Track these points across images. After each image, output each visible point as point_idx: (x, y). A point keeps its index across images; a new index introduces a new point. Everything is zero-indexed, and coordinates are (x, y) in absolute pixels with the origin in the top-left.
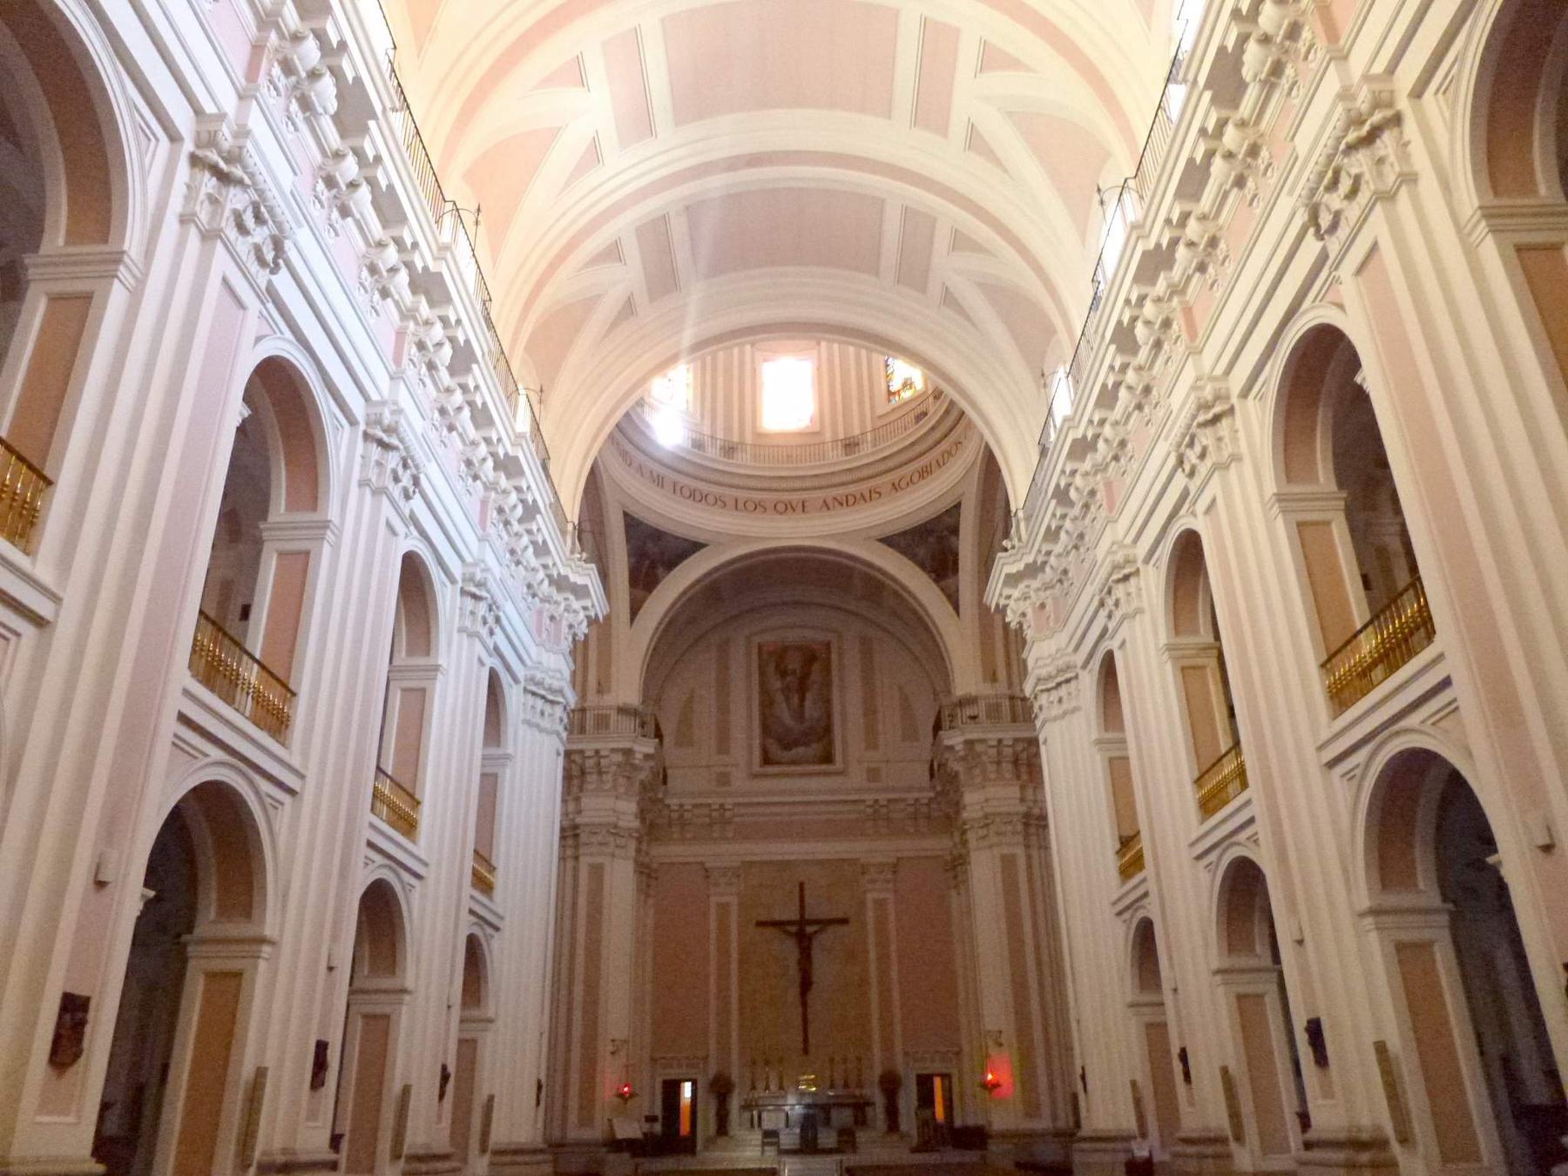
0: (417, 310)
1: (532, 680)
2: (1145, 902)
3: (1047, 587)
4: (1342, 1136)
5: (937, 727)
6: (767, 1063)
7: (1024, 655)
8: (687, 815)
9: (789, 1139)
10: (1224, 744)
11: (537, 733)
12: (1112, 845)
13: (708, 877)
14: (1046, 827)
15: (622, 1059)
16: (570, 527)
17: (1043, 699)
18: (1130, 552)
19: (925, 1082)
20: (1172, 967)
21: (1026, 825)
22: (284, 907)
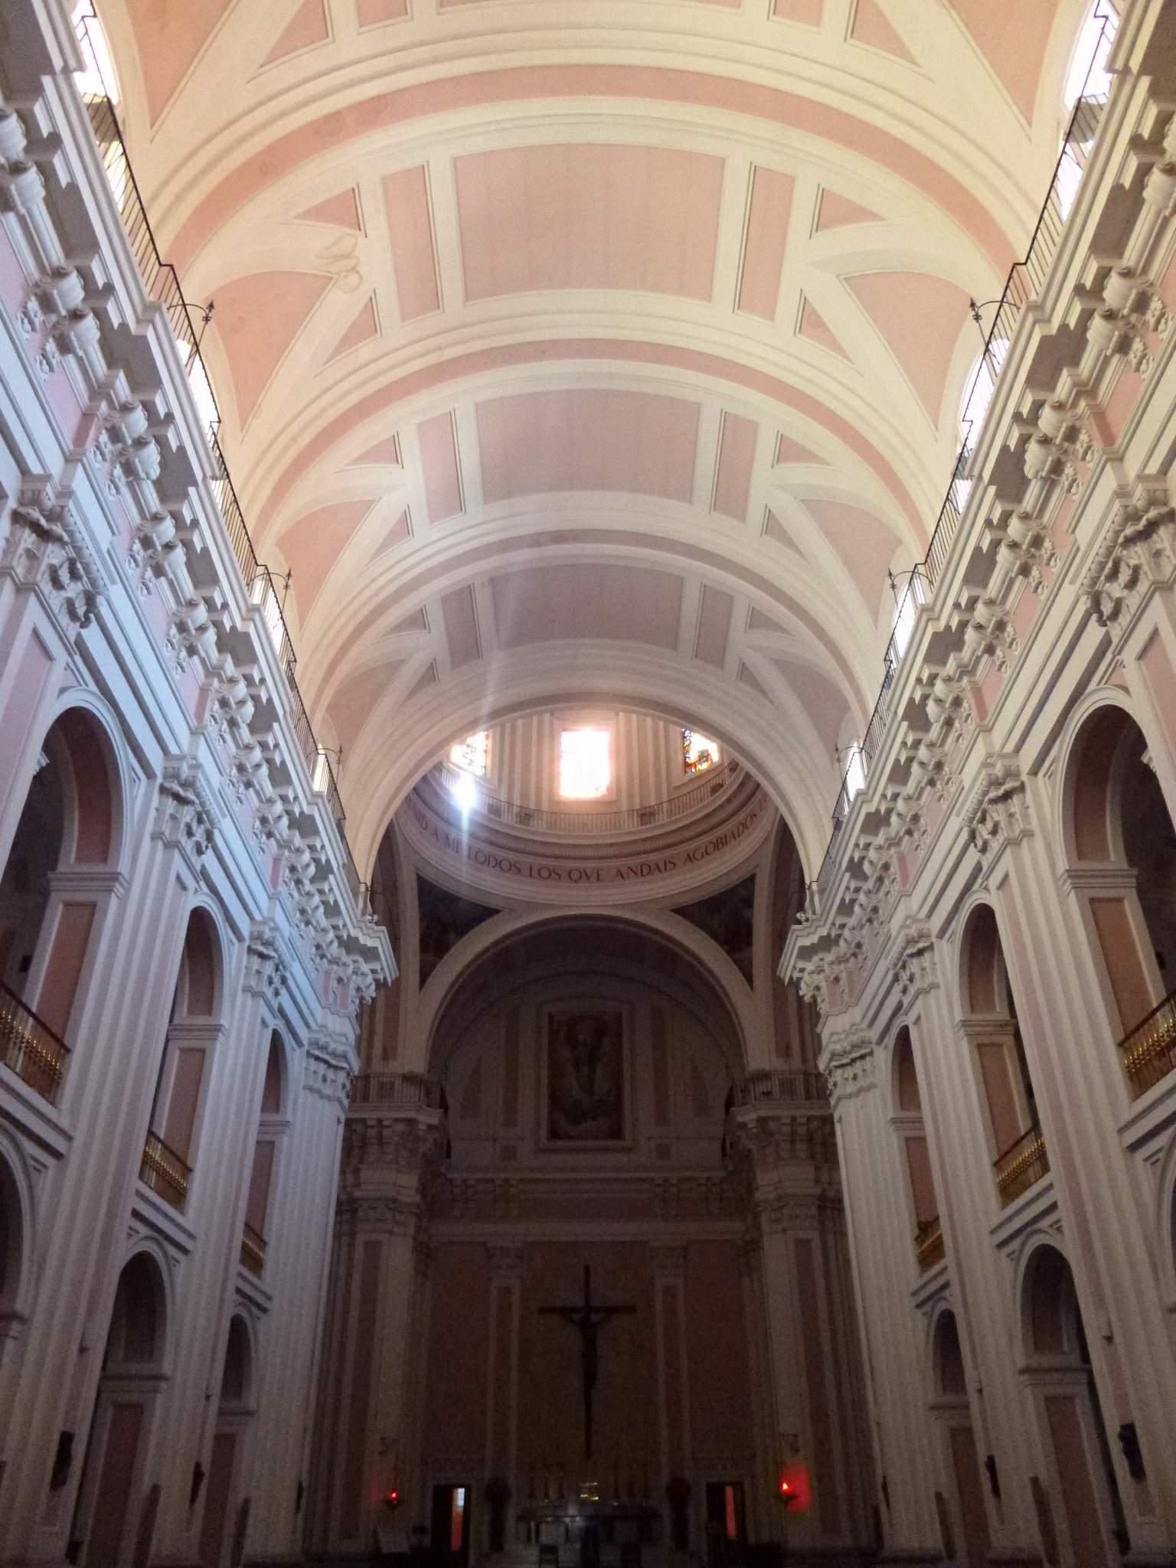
0: (112, 385)
1: (315, 1044)
2: (947, 1293)
3: (840, 960)
5: (729, 1103)
7: (818, 1030)
10: (1023, 1125)
13: (489, 1258)
16: (362, 888)
17: (838, 1075)
20: (976, 1367)
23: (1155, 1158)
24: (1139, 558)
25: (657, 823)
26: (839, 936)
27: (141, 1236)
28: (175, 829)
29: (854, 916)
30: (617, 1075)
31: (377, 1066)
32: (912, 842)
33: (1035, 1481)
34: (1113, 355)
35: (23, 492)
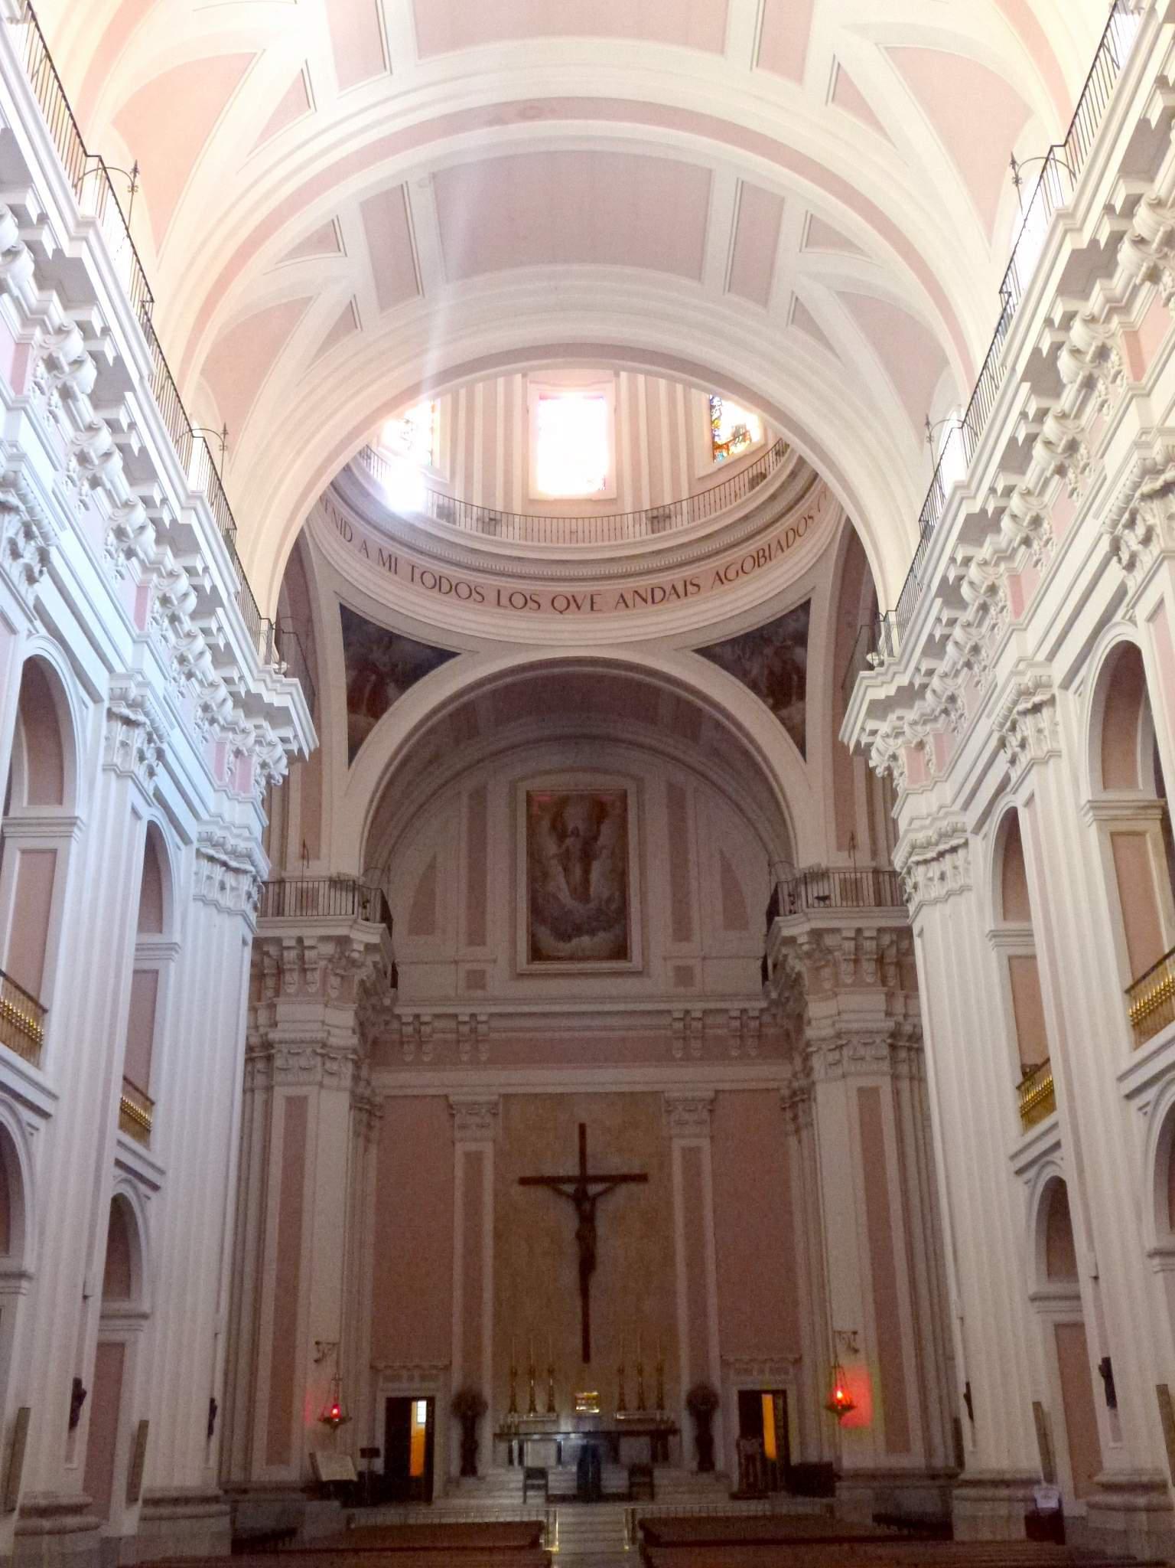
1: (209, 839)
2: (1055, 1156)
3: (927, 719)
5: (773, 912)
6: (532, 1373)
7: (893, 814)
9: (562, 1479)
11: (215, 911)
12: (1010, 1076)
13: (452, 1116)
14: (920, 1050)
15: (329, 1369)
17: (919, 875)
19: (750, 1402)
24: (1154, 516)
30: (621, 877)
32: (1031, 555)
34: (1141, 284)
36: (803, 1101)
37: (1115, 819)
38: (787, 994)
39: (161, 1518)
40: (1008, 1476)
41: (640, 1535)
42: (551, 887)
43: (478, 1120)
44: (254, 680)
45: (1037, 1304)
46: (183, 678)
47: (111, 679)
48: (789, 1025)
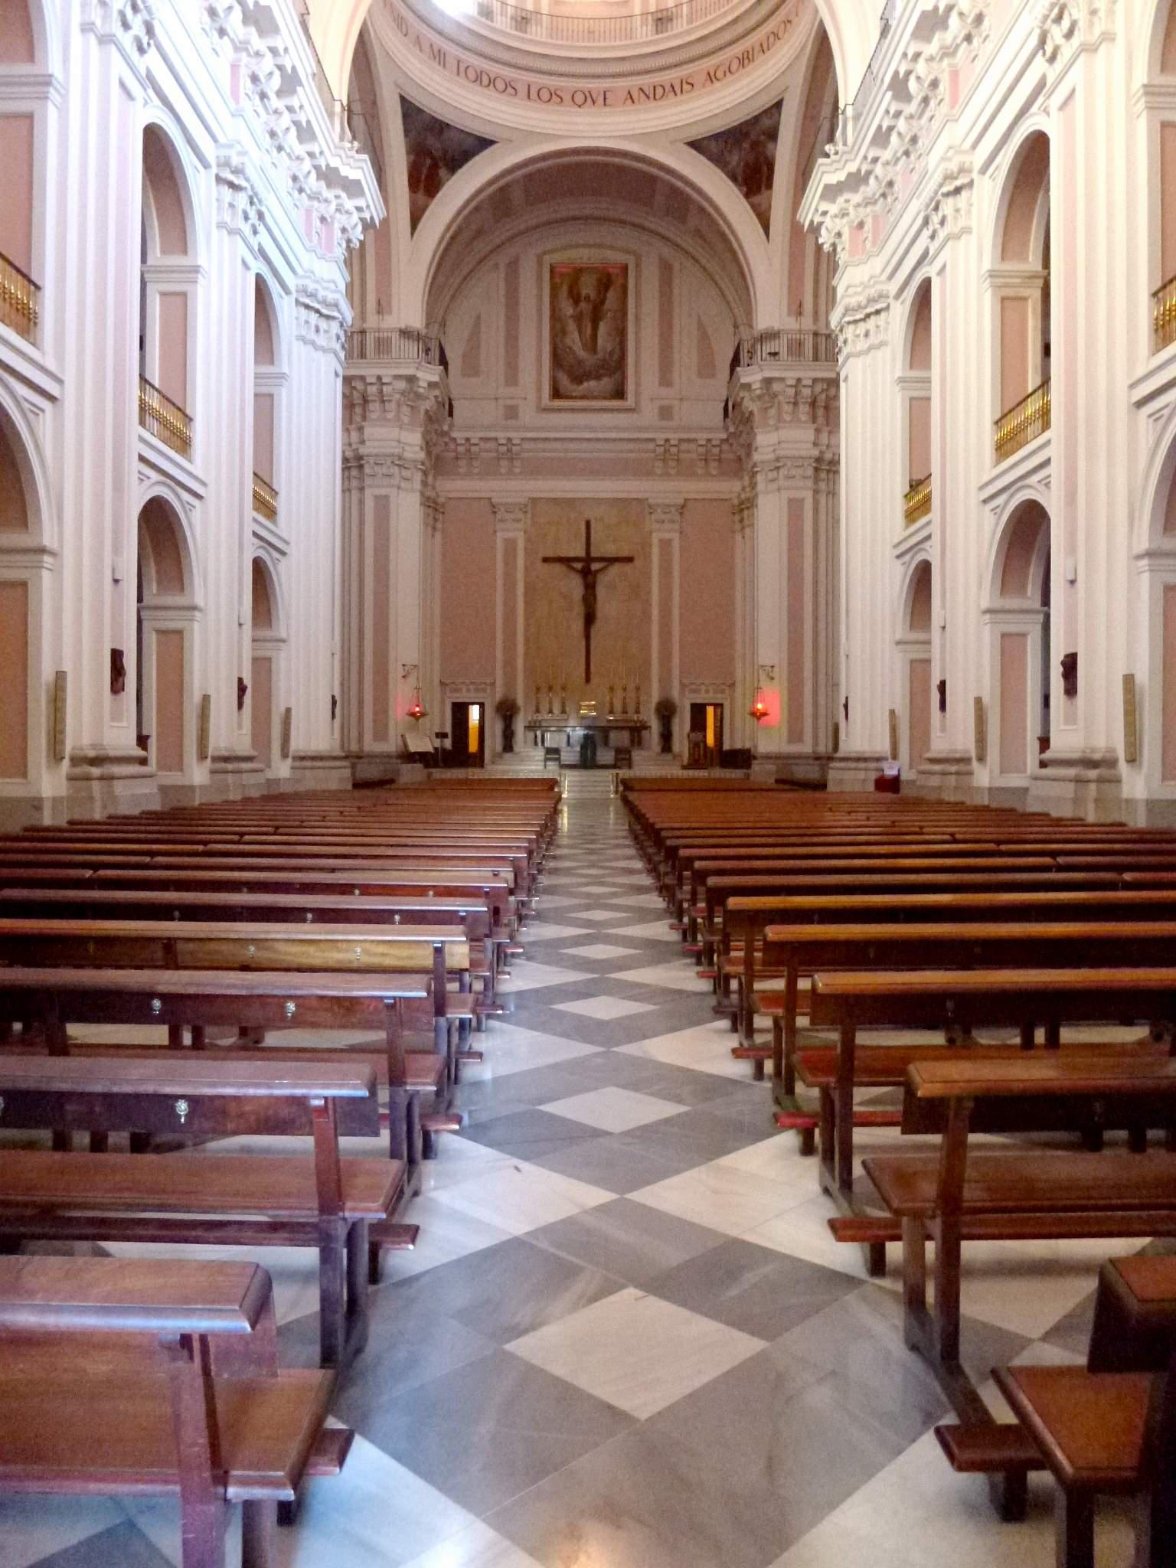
1: (304, 291)
2: (926, 545)
3: (869, 202)
4: (1076, 755)
5: (735, 362)
6: (550, 688)
7: (834, 283)
8: (474, 449)
9: (570, 756)
10: (1033, 381)
11: (312, 350)
12: (900, 487)
13: (495, 512)
14: (837, 472)
15: (412, 680)
16: (338, 108)
17: (850, 332)
18: (966, 159)
19: (698, 711)
20: (943, 607)
21: (816, 470)
22: (60, 518)
23: (1157, 416)
25: (675, 32)
26: (869, 173)
27: (152, 481)
28: (106, 17)
29: (950, 30)
30: (621, 333)
31: (372, 321)
32: (970, 51)
33: (1129, 680)
35: (218, 157)
36: (748, 508)
37: (1006, 286)
38: (740, 428)
39: (305, 768)
40: (867, 755)
41: (621, 788)
42: (568, 341)
43: (512, 516)
44: (332, 155)
45: (900, 647)
46: (275, 151)
47: (217, 148)
48: (742, 452)
